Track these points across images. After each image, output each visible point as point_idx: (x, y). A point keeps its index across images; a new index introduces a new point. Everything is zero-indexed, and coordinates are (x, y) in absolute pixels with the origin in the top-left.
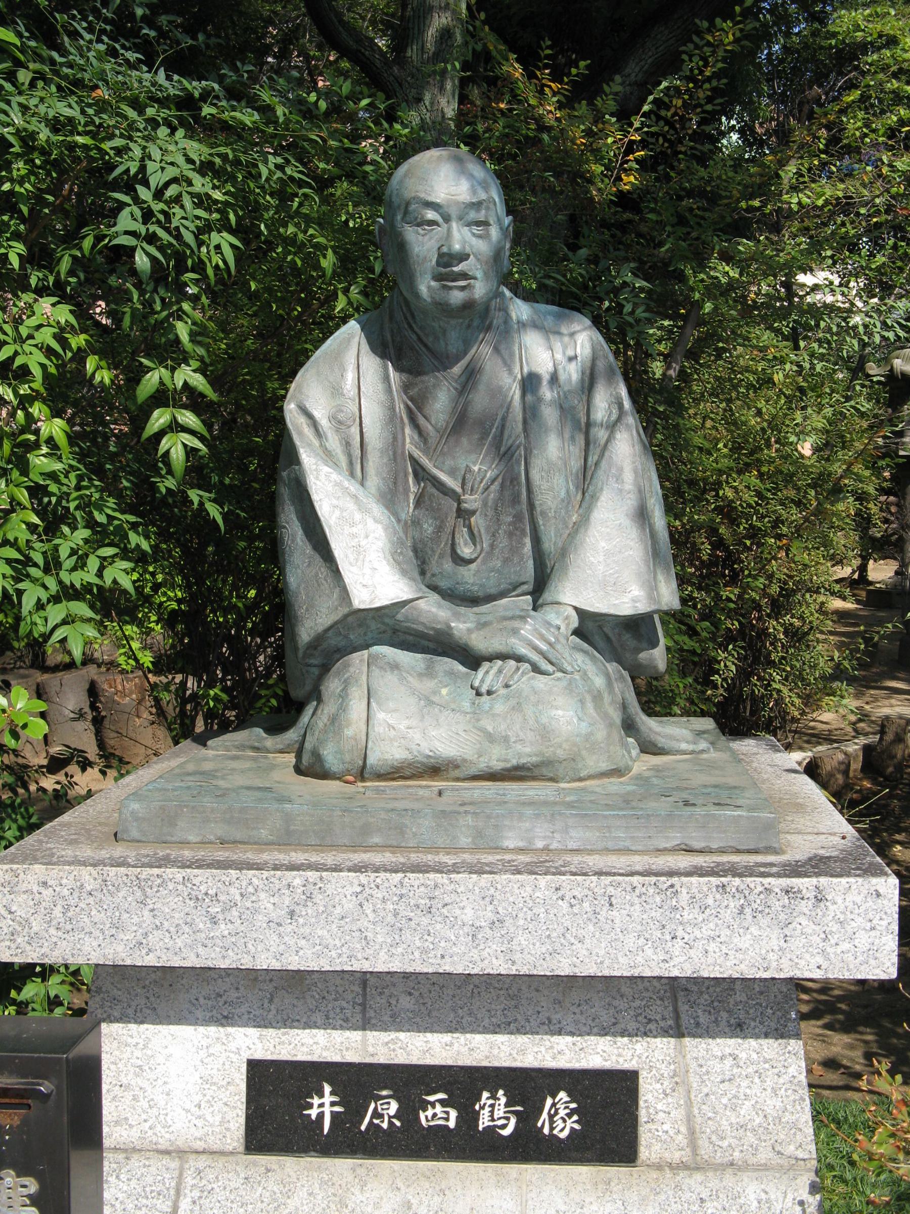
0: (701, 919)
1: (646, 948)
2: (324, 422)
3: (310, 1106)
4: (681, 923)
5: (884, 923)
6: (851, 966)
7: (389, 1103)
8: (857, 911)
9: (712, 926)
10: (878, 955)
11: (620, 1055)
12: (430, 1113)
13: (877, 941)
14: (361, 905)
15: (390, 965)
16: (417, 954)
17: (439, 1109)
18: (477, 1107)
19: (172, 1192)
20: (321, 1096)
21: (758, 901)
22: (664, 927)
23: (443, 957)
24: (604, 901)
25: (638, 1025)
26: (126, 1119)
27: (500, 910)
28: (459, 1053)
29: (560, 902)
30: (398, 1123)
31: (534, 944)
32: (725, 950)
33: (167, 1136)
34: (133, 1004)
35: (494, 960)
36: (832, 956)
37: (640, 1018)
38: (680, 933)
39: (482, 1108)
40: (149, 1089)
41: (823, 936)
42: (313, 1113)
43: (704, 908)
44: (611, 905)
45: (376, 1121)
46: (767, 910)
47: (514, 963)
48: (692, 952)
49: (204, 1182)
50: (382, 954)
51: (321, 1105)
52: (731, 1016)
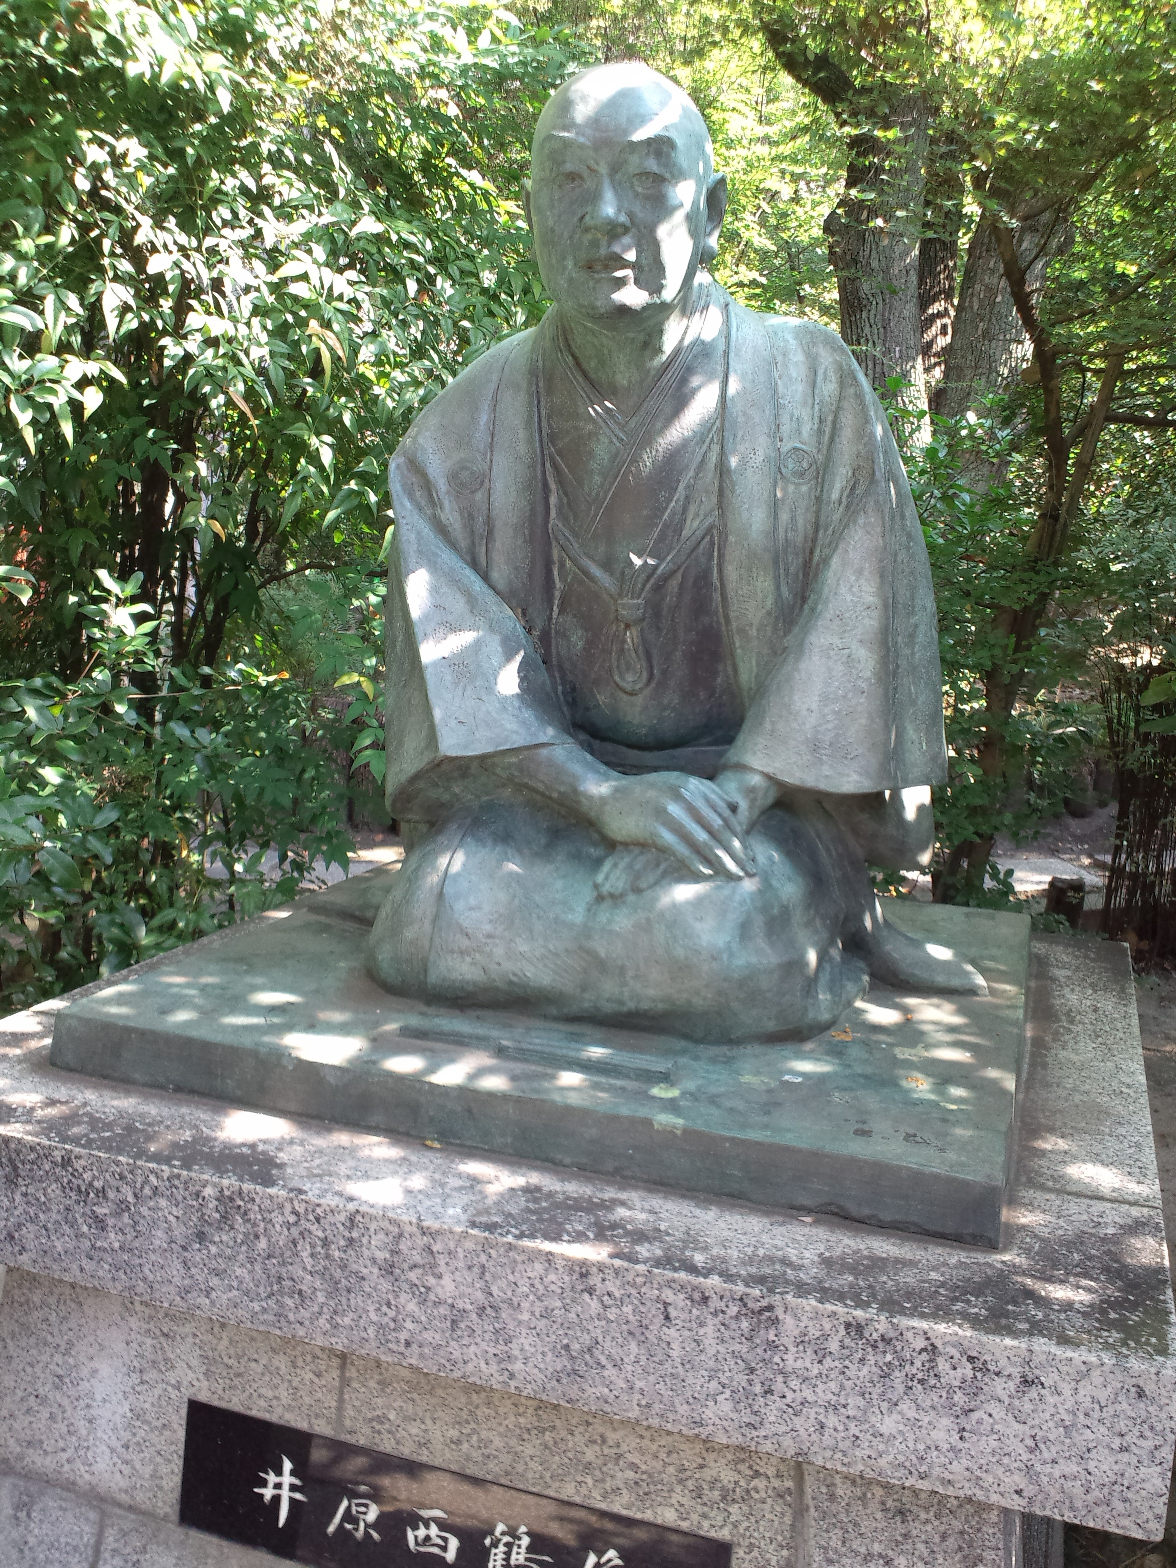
0: (815, 1372)
1: (720, 1398)
2: (442, 485)
3: (264, 1483)
4: (781, 1372)
5: (1148, 1444)
6: (1078, 1504)
7: (366, 1506)
8: (1096, 1415)
9: (833, 1386)
10: (1130, 1495)
11: (704, 1516)
12: (422, 1532)
13: (1130, 1472)
14: (294, 1243)
15: (333, 1340)
16: (371, 1331)
17: (434, 1530)
18: (488, 1542)
19: (90, 1552)
20: (279, 1472)
21: (918, 1364)
22: (752, 1371)
23: (408, 1344)
24: (653, 1310)
25: (737, 1477)
26: (41, 1442)
27: (495, 1290)
28: (468, 1458)
29: (586, 1296)
30: (375, 1535)
31: (543, 1354)
32: (854, 1430)
33: (87, 1477)
34: (57, 1291)
35: (483, 1366)
36: (1045, 1479)
37: (741, 1467)
38: (779, 1385)
39: (495, 1544)
40: (69, 1409)
41: (1029, 1442)
42: (268, 1493)
43: (821, 1355)
44: (667, 1318)
45: (348, 1526)
46: (933, 1381)
47: (512, 1376)
48: (798, 1422)
49: (128, 1550)
50: (322, 1321)
51: (278, 1486)
52: (888, 1494)
